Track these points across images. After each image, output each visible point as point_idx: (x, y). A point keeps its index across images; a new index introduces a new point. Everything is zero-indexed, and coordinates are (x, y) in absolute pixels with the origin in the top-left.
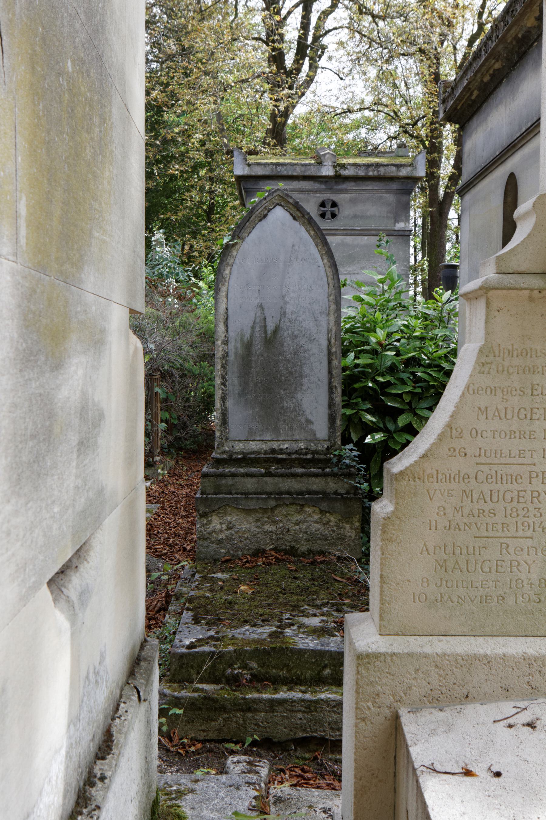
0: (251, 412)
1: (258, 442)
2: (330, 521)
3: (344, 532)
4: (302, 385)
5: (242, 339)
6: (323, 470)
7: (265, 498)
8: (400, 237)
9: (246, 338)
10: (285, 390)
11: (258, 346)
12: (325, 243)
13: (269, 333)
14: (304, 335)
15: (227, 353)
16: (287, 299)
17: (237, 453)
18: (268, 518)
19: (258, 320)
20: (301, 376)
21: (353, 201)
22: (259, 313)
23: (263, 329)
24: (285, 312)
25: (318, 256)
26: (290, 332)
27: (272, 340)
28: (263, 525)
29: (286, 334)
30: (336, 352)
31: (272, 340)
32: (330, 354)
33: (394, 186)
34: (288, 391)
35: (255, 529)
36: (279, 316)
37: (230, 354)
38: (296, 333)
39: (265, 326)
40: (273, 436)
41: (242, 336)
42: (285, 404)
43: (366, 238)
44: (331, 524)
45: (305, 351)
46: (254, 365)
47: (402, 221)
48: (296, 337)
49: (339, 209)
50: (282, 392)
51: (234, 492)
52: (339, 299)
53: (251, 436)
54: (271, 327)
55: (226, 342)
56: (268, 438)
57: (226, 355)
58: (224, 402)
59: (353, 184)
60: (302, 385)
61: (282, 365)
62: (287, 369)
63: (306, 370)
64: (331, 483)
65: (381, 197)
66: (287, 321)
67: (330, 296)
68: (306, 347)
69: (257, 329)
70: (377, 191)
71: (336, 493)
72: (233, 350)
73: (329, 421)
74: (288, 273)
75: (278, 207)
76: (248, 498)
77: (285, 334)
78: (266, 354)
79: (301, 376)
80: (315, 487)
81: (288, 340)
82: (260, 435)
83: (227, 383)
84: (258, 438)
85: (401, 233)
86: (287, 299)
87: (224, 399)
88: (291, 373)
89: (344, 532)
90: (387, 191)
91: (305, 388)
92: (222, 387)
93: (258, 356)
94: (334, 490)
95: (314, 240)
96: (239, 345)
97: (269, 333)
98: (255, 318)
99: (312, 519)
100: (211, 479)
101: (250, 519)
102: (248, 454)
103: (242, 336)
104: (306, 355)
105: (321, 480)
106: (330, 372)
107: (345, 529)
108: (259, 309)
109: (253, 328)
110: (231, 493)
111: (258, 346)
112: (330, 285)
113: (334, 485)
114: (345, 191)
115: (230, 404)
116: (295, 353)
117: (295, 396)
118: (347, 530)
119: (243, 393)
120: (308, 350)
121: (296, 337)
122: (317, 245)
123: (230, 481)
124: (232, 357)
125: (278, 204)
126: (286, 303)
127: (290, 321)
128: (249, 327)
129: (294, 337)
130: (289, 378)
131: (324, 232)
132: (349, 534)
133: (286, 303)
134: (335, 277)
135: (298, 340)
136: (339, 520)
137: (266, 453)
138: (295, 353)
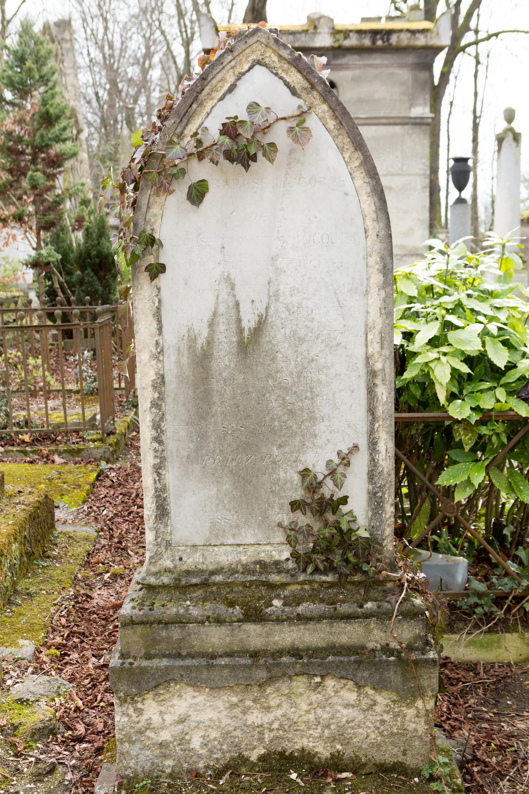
0: (214, 491)
1: (229, 548)
2: (375, 703)
3: (403, 723)
4: (315, 436)
5: (191, 348)
6: (361, 606)
7: (245, 666)
8: (417, 127)
9: (199, 346)
10: (280, 446)
11: (224, 358)
12: (359, 145)
13: (246, 333)
14: (317, 338)
15: (163, 377)
16: (281, 263)
17: (188, 573)
18: (254, 701)
19: (222, 309)
20: (313, 419)
21: (356, 80)
22: (224, 295)
23: (233, 326)
24: (278, 291)
25: (344, 171)
26: (288, 331)
27: (250, 342)
28: (244, 713)
29: (278, 335)
30: (383, 369)
31: (250, 342)
32: (372, 374)
33: (410, 59)
34: (287, 449)
35: (229, 721)
36: (265, 301)
37: (167, 379)
38: (301, 333)
39: (239, 320)
40: (260, 536)
41: (193, 340)
42: (282, 474)
43: (373, 128)
44: (378, 709)
45: (320, 370)
46: (216, 399)
47: (420, 105)
48: (302, 340)
49: (338, 92)
50: (275, 451)
51: (184, 653)
52: (388, 261)
53: (217, 536)
54: (249, 322)
55: (159, 353)
56: (251, 540)
57: (160, 383)
58: (159, 475)
59: (356, 57)
60: (315, 436)
61: (273, 397)
62: (284, 404)
63: (323, 407)
64: (375, 632)
65: (393, 74)
66: (281, 308)
67: (368, 255)
68: (321, 361)
69: (222, 327)
70: (387, 66)
71: (386, 650)
72: (175, 371)
73: (369, 505)
74: (282, 210)
75: (257, 67)
76: (213, 666)
77: (280, 336)
78: (242, 376)
79: (313, 419)
80: (344, 640)
81: (285, 348)
82: (234, 536)
83: (164, 438)
84: (230, 541)
85: (418, 121)
86: (281, 263)
87: (158, 469)
88: (291, 413)
89: (403, 723)
90: (401, 66)
91: (319, 441)
92: (156, 445)
93: (225, 381)
94: (383, 643)
95: (334, 138)
96: (185, 360)
97: (246, 333)
98: (217, 303)
99: (340, 701)
100: (139, 629)
101: (219, 704)
102: (213, 573)
103: (193, 340)
104: (323, 377)
105: (356, 626)
106: (371, 411)
107: (405, 716)
108: (223, 285)
109: (212, 325)
110: (179, 656)
111: (224, 358)
112: (370, 232)
113: (383, 635)
114: (346, 67)
115: (171, 476)
116: (300, 375)
117: (303, 459)
118: (408, 718)
119: (195, 456)
120: (327, 367)
121: (302, 340)
122: (341, 150)
123: (176, 633)
124: (171, 384)
125: (259, 63)
126: (279, 271)
127: (288, 310)
128: (205, 324)
129: (297, 340)
130: (289, 423)
131: (356, 122)
132: (413, 726)
133: (279, 271)
134: (381, 215)
135: (304, 347)
136: (394, 702)
137: (247, 570)
138: (300, 375)
